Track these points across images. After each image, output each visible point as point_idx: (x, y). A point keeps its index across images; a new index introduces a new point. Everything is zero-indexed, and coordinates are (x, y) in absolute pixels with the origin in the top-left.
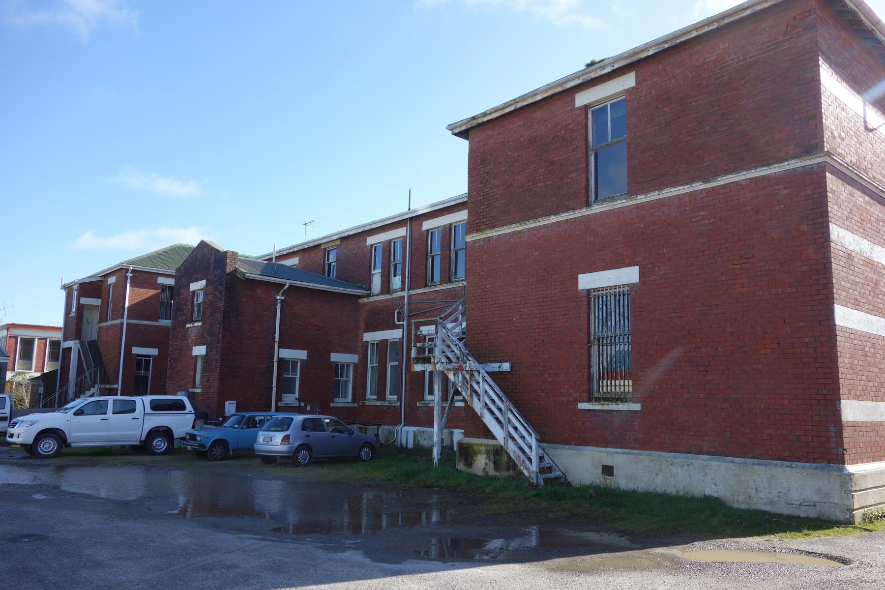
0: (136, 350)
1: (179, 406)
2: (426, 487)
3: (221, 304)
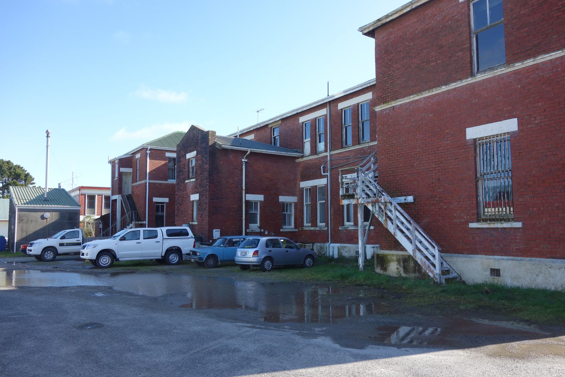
0: (155, 200)
1: (185, 234)
2: (358, 285)
3: (207, 166)
